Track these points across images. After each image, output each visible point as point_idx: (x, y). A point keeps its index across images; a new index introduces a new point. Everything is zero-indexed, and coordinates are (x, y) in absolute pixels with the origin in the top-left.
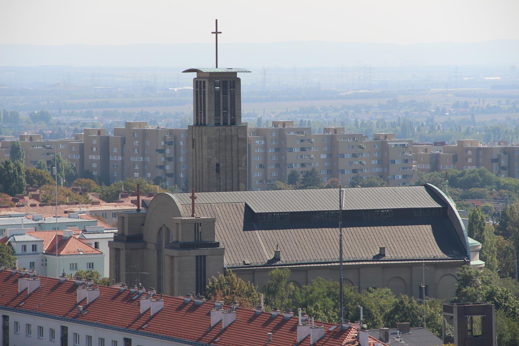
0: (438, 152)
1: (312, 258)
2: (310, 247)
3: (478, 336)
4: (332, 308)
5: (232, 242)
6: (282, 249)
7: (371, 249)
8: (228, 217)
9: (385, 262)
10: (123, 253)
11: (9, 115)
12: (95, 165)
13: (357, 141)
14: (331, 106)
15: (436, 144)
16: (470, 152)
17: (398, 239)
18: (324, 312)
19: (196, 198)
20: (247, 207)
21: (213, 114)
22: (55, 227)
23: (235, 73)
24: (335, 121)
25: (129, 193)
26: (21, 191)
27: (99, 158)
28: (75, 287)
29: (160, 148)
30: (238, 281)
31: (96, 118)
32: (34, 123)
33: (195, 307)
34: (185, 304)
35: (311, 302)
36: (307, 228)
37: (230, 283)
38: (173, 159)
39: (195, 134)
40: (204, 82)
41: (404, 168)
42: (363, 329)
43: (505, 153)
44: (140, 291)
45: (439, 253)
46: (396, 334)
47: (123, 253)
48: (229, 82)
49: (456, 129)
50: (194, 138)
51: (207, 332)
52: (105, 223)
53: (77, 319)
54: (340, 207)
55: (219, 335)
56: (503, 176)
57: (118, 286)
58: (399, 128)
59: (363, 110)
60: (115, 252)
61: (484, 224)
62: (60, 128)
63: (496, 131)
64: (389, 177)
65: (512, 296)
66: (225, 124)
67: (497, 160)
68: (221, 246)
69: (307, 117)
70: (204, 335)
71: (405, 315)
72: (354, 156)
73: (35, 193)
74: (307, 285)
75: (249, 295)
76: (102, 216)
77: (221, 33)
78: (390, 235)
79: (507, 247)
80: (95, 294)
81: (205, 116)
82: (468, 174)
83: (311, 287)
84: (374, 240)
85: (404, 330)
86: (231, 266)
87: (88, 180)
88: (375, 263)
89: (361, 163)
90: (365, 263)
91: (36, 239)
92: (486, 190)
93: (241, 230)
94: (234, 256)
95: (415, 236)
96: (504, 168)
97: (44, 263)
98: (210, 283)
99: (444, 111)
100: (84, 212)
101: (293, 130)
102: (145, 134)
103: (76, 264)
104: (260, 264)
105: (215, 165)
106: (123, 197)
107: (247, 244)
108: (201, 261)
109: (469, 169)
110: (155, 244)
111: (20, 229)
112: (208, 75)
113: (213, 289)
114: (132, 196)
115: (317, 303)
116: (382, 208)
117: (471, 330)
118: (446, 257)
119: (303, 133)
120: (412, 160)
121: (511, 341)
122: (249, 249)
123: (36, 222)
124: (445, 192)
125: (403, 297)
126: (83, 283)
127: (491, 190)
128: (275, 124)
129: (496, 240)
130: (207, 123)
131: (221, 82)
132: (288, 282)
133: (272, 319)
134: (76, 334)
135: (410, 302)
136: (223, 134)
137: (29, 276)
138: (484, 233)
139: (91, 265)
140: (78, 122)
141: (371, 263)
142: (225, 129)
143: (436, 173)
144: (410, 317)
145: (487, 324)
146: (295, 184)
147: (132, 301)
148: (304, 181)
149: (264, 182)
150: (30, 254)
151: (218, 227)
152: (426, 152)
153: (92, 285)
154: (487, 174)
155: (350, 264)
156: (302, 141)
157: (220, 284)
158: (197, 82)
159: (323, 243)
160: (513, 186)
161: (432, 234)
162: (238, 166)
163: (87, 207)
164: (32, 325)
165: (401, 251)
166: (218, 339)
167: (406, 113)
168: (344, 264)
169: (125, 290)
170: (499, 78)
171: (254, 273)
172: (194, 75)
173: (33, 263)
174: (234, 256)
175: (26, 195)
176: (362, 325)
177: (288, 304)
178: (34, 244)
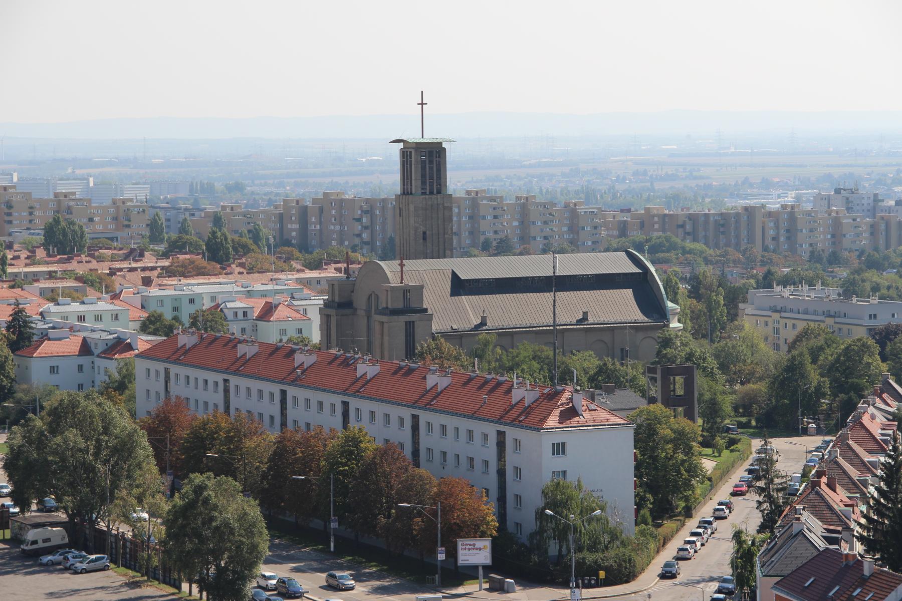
0: (625, 218)
1: (518, 323)
2: (515, 312)
3: (680, 396)
4: (538, 371)
5: (440, 309)
6: (489, 315)
7: (575, 313)
8: (436, 284)
9: (588, 326)
10: (333, 320)
11: (206, 186)
12: (294, 234)
13: (548, 208)
14: (515, 175)
15: (622, 211)
16: (656, 219)
17: (601, 304)
18: (530, 374)
19: (404, 265)
20: (454, 274)
21: (419, 183)
22: (264, 294)
23: (441, 143)
24: (520, 189)
25: (331, 260)
26: (228, 259)
27: (297, 226)
28: (292, 352)
29: (357, 217)
30: (447, 346)
31: (288, 188)
32: (229, 193)
33: (410, 371)
34: (400, 368)
35: (518, 365)
36: (512, 293)
37: (438, 348)
38: (370, 228)
39: (402, 203)
40: (411, 152)
41: (593, 234)
42: (577, 391)
43: (690, 219)
44: (357, 356)
45: (639, 316)
46: (602, 395)
47: (333, 320)
48: (435, 152)
49: (638, 196)
50: (401, 206)
51: (423, 395)
52: (310, 289)
53: (295, 382)
54: (554, 273)
55: (434, 398)
56: (688, 241)
57: (334, 351)
58: (582, 196)
59: (546, 178)
60: (326, 319)
61: (678, 288)
62: (255, 198)
63: (676, 197)
64: (579, 243)
65: (709, 357)
66: (431, 193)
67: (682, 226)
68: (430, 312)
69: (493, 186)
70: (420, 398)
71: (608, 376)
72: (545, 223)
73: (241, 261)
74: (513, 348)
75: (457, 359)
76: (307, 283)
77: (426, 104)
78: (592, 300)
79: (700, 310)
80: (313, 359)
81: (411, 185)
82: (655, 239)
83: (517, 351)
84: (577, 305)
85: (609, 391)
86: (439, 331)
87: (290, 249)
88: (578, 327)
89: (551, 230)
90: (568, 327)
91: (247, 306)
92: (672, 255)
93: (449, 296)
94: (442, 322)
95: (616, 300)
96: (688, 234)
97: (255, 329)
98: (419, 348)
99: (624, 179)
100: (290, 280)
101: (486, 198)
102: (342, 203)
103: (285, 330)
104: (467, 329)
105: (422, 233)
106: (327, 264)
107: (454, 309)
108: (410, 328)
109: (655, 234)
110: (364, 310)
111: (230, 295)
112: (414, 146)
113: (422, 353)
114: (335, 263)
115: (523, 366)
116: (585, 273)
117: (674, 390)
118: (646, 319)
119: (495, 201)
120: (601, 226)
121: (712, 399)
122: (457, 314)
123: (245, 290)
124: (644, 256)
125: (606, 359)
126: (300, 348)
127: (677, 254)
128: (468, 192)
129: (689, 303)
130: (413, 192)
131: (427, 152)
132: (495, 346)
133: (486, 382)
134: (516, 440)
135: (614, 364)
136: (430, 203)
137: (247, 342)
138: (678, 296)
139: (300, 331)
140: (272, 192)
141: (575, 327)
142: (431, 198)
143: (623, 239)
144: (613, 378)
145: (689, 384)
146: (489, 251)
147: (348, 365)
148: (497, 248)
149: (458, 249)
150: (241, 320)
151: (426, 294)
152: (614, 218)
153: (309, 350)
154: (673, 240)
155: (545, 328)
156: (494, 209)
157: (429, 349)
158: (403, 152)
159: (527, 308)
160: (698, 250)
161: (633, 298)
162: (444, 234)
163: (292, 275)
164: (190, 377)
165: (603, 315)
166: (435, 402)
167: (588, 181)
168: (558, 327)
169: (342, 355)
170: (675, 147)
171: (461, 339)
172: (401, 145)
173: (244, 329)
174: (442, 322)
175: (233, 263)
176: (575, 387)
177: (495, 367)
178: (245, 310)
